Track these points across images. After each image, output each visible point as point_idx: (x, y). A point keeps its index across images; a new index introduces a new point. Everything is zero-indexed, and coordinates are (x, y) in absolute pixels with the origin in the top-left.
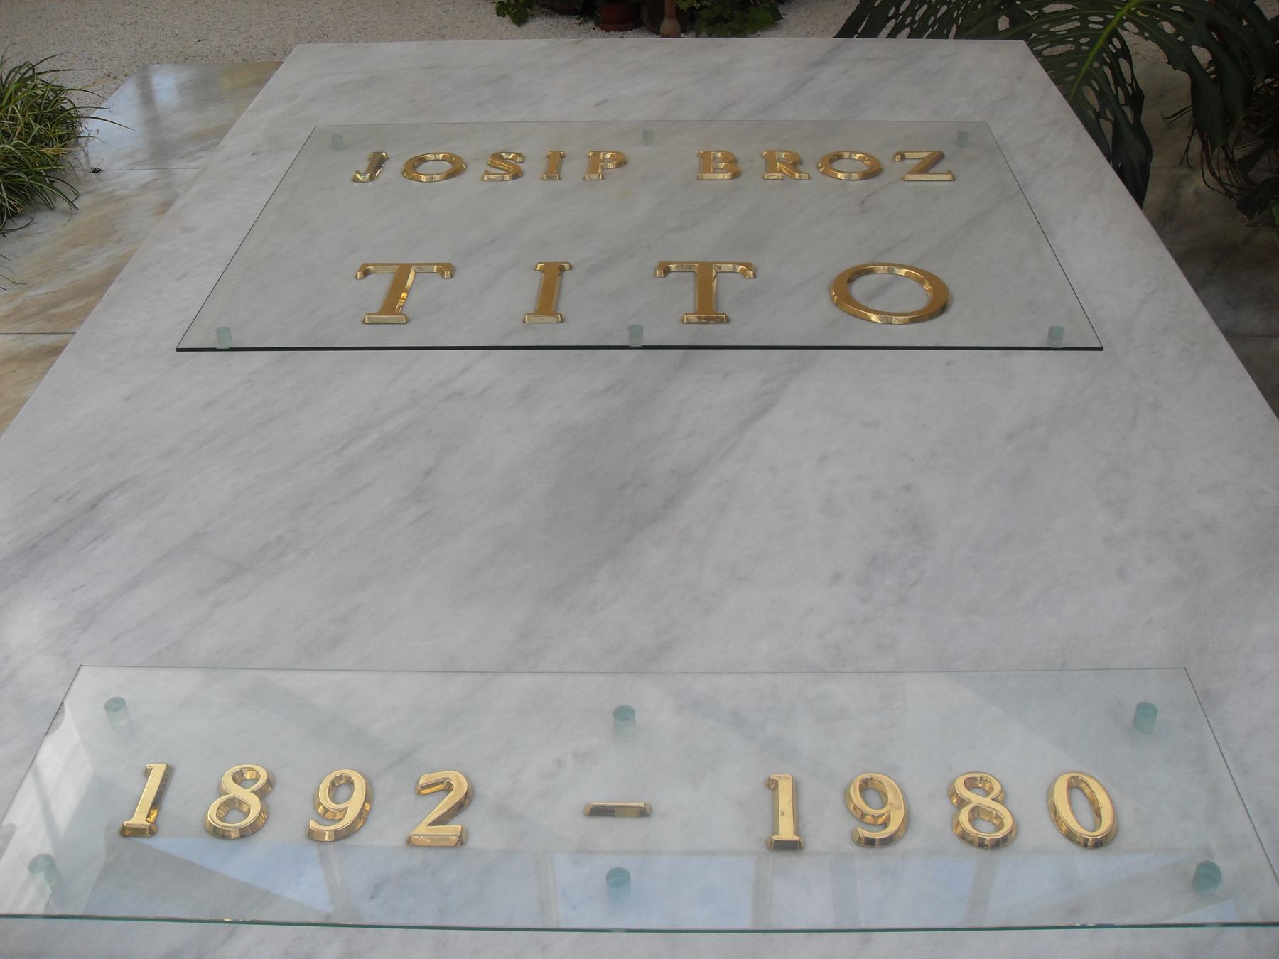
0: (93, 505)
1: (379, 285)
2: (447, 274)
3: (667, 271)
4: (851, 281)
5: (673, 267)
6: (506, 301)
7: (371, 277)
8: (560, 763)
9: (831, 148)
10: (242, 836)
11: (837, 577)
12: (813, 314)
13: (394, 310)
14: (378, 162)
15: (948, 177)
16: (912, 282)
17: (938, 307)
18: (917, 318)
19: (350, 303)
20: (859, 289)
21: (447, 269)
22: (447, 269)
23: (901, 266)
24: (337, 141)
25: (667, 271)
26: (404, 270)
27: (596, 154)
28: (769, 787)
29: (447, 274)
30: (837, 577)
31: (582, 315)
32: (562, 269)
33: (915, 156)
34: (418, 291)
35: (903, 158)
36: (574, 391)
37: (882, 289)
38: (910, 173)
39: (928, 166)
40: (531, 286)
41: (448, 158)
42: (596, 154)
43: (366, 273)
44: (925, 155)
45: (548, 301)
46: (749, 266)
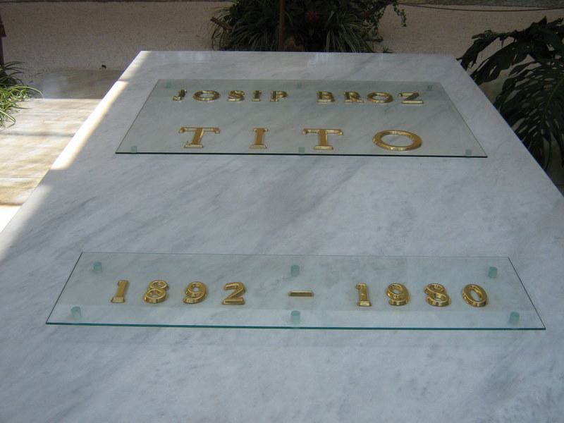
0: (83, 204)
1: (189, 136)
2: (217, 132)
3: (307, 132)
4: (381, 137)
5: (310, 131)
6: (245, 141)
7: (185, 133)
8: (278, 281)
9: (371, 91)
10: (157, 302)
11: (379, 228)
12: (370, 147)
13: (196, 144)
14: (182, 94)
15: (421, 102)
16: (406, 137)
17: (417, 144)
18: (409, 148)
19: (179, 141)
20: (384, 139)
21: (216, 130)
22: (216, 130)
23: (393, 146)
24: (169, 85)
25: (307, 132)
26: (199, 131)
27: (275, 92)
28: (429, 87)
29: (217, 132)
30: (379, 228)
31: (271, 144)
32: (264, 131)
33: (407, 95)
34: (206, 137)
35: (402, 95)
36: (272, 171)
37: (394, 139)
38: (406, 100)
39: (411, 98)
40: (253, 137)
41: (213, 92)
42: (275, 92)
43: (184, 131)
44: (230, 4)
45: (259, 141)
46: (340, 131)
